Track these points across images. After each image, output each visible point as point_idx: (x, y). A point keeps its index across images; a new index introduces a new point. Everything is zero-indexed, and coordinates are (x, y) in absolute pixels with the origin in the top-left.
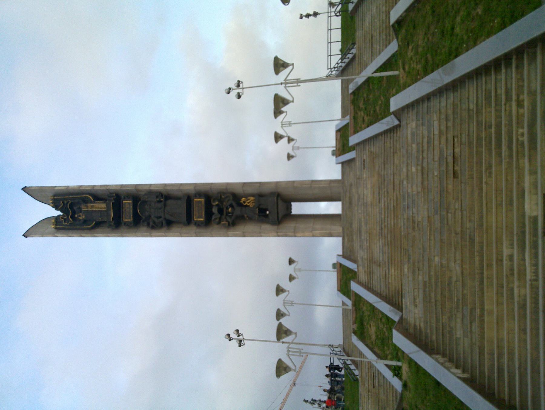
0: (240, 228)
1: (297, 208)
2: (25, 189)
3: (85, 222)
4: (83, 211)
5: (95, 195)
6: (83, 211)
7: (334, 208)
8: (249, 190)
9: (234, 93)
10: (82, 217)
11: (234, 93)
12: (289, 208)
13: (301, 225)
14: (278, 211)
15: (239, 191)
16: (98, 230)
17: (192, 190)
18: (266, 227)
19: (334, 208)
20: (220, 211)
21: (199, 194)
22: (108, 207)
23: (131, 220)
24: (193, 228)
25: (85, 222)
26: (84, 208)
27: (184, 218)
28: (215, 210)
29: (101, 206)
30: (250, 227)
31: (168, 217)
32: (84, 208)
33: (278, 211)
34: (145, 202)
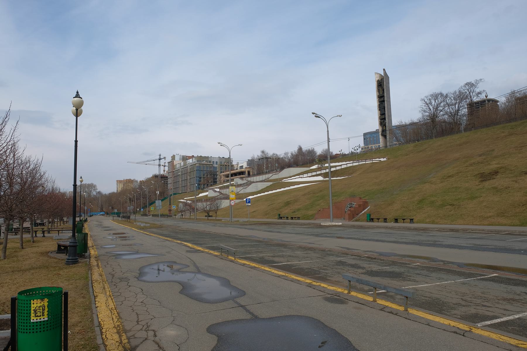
4: (382, 85)
6: (382, 85)
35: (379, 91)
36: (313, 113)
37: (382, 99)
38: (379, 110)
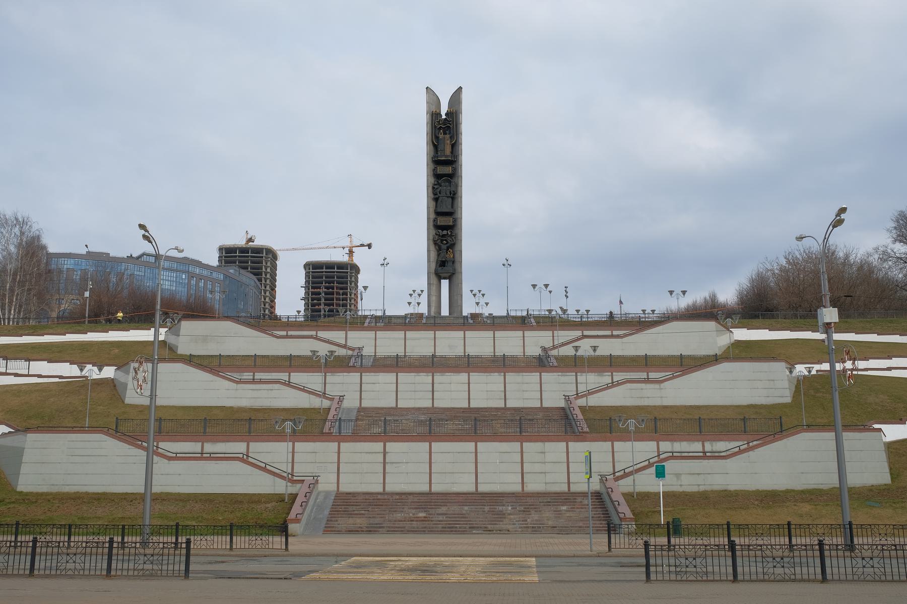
0: (432, 247)
1: (445, 283)
2: (460, 88)
3: (437, 138)
4: (444, 131)
5: (455, 145)
6: (444, 131)
7: (445, 312)
8: (457, 256)
9: (505, 262)
10: (441, 136)
11: (505, 262)
12: (445, 278)
13: (434, 288)
14: (315, 249)
15: (457, 248)
16: (432, 146)
17: (430, 125)
18: (433, 266)
19: (445, 312)
20: (443, 236)
21: (455, 220)
22: (446, 156)
23: (439, 172)
24: (433, 216)
25: (437, 138)
26: (448, 136)
27: (439, 210)
28: (445, 232)
29: (448, 151)
30: (434, 254)
31: (440, 199)
32: (448, 136)
33: (315, 249)
34: (450, 182)
35: (435, 143)
36: (142, 227)
37: (448, 170)
38: (436, 200)
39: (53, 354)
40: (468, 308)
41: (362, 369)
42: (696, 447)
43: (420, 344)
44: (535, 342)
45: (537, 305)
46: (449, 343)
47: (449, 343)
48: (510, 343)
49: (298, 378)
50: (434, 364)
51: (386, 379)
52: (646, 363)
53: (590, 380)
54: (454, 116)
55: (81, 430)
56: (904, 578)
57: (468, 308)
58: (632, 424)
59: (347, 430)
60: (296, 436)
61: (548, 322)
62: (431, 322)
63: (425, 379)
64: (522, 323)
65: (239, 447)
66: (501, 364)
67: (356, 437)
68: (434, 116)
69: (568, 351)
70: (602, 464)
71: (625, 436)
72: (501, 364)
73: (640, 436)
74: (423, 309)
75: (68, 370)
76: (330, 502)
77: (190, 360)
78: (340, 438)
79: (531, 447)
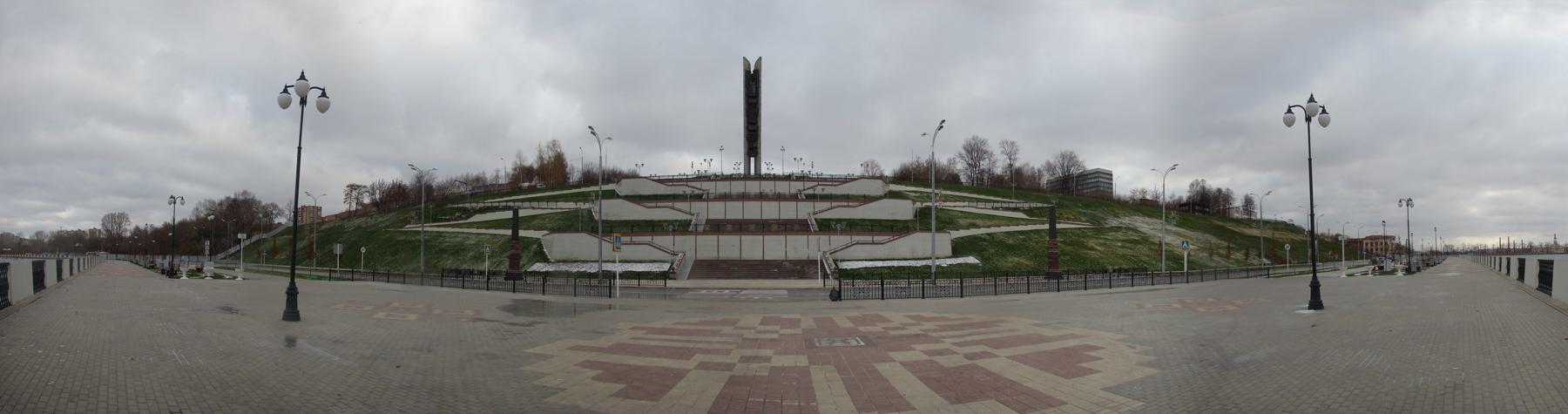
4: (752, 81)
6: (752, 81)
39: (566, 198)
40: (764, 171)
41: (708, 200)
42: (869, 238)
43: (738, 188)
44: (795, 187)
45: (795, 169)
46: (753, 187)
47: (753, 187)
48: (783, 188)
49: (678, 205)
50: (744, 197)
51: (720, 205)
52: (847, 198)
53: (821, 205)
54: (757, 72)
55: (577, 231)
56: (20, 273)
57: (764, 171)
58: (752, 227)
59: (701, 229)
60: (675, 232)
61: (802, 178)
62: (746, 177)
63: (775, 204)
64: (788, 178)
65: (648, 239)
66: (779, 197)
67: (705, 232)
68: (747, 72)
69: (810, 192)
70: (825, 247)
71: (835, 232)
72: (779, 197)
73: (843, 232)
74: (742, 171)
75: (572, 205)
76: (220, 256)
77: (627, 198)
78: (696, 233)
79: (790, 238)
